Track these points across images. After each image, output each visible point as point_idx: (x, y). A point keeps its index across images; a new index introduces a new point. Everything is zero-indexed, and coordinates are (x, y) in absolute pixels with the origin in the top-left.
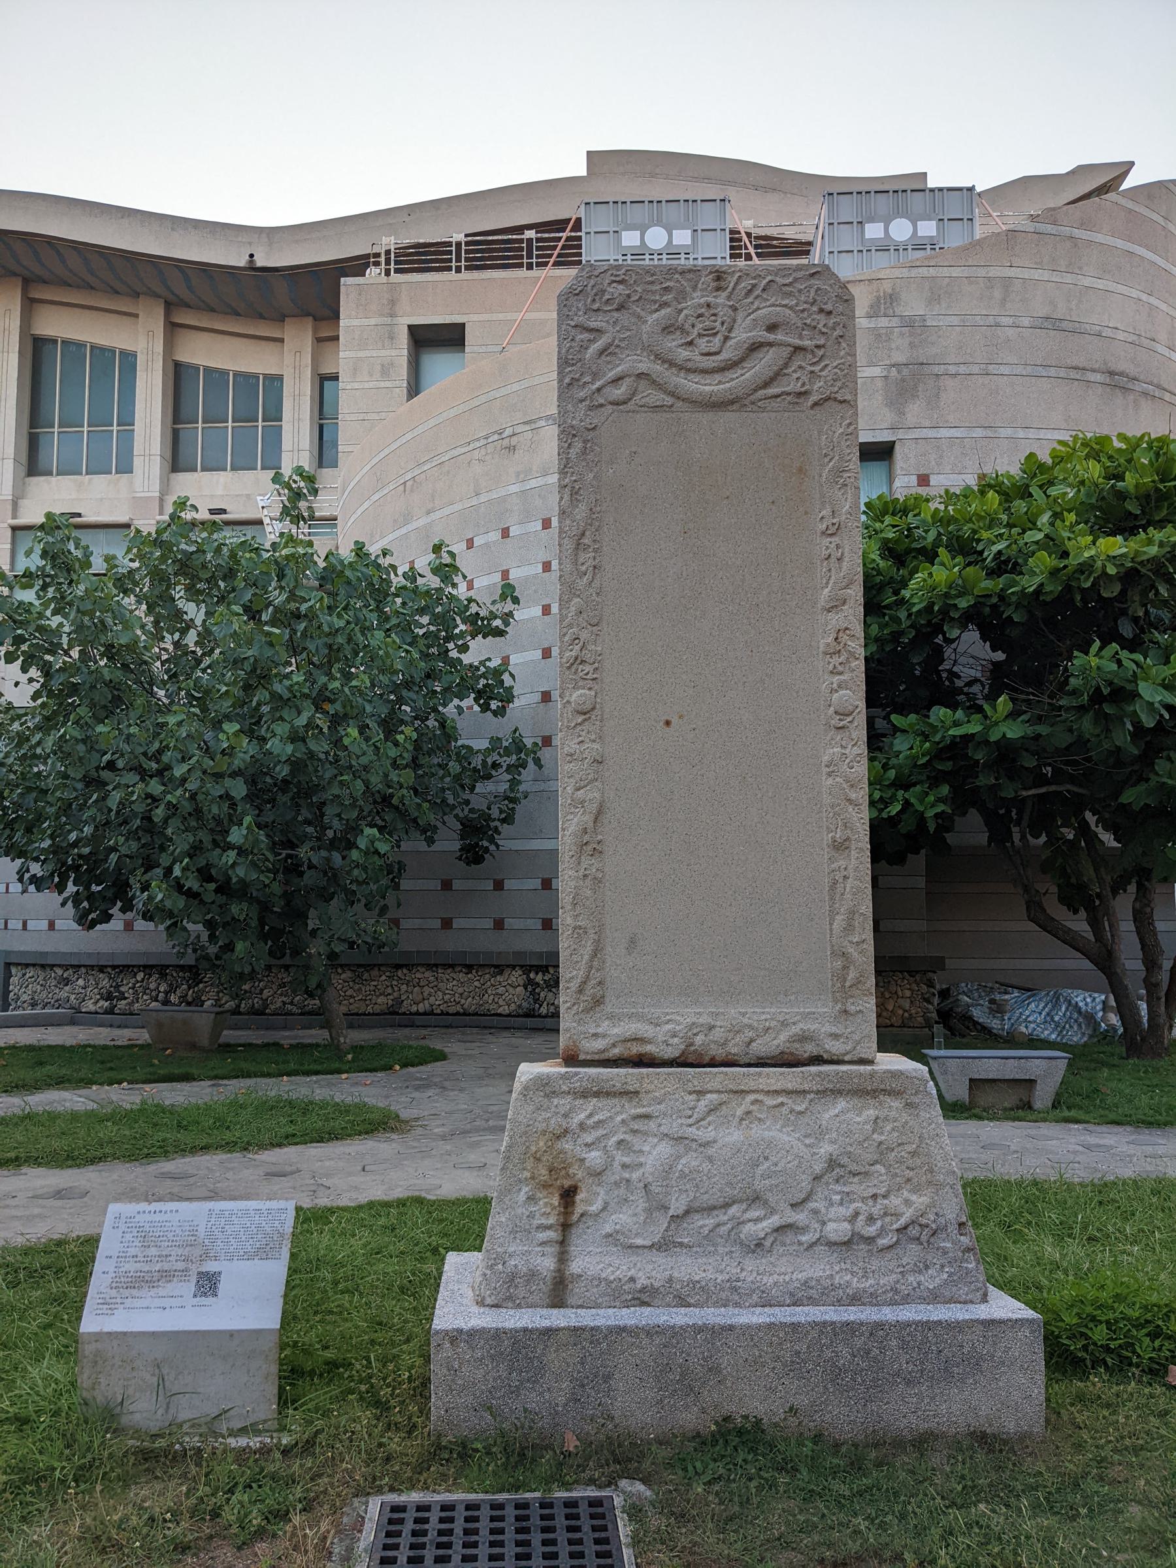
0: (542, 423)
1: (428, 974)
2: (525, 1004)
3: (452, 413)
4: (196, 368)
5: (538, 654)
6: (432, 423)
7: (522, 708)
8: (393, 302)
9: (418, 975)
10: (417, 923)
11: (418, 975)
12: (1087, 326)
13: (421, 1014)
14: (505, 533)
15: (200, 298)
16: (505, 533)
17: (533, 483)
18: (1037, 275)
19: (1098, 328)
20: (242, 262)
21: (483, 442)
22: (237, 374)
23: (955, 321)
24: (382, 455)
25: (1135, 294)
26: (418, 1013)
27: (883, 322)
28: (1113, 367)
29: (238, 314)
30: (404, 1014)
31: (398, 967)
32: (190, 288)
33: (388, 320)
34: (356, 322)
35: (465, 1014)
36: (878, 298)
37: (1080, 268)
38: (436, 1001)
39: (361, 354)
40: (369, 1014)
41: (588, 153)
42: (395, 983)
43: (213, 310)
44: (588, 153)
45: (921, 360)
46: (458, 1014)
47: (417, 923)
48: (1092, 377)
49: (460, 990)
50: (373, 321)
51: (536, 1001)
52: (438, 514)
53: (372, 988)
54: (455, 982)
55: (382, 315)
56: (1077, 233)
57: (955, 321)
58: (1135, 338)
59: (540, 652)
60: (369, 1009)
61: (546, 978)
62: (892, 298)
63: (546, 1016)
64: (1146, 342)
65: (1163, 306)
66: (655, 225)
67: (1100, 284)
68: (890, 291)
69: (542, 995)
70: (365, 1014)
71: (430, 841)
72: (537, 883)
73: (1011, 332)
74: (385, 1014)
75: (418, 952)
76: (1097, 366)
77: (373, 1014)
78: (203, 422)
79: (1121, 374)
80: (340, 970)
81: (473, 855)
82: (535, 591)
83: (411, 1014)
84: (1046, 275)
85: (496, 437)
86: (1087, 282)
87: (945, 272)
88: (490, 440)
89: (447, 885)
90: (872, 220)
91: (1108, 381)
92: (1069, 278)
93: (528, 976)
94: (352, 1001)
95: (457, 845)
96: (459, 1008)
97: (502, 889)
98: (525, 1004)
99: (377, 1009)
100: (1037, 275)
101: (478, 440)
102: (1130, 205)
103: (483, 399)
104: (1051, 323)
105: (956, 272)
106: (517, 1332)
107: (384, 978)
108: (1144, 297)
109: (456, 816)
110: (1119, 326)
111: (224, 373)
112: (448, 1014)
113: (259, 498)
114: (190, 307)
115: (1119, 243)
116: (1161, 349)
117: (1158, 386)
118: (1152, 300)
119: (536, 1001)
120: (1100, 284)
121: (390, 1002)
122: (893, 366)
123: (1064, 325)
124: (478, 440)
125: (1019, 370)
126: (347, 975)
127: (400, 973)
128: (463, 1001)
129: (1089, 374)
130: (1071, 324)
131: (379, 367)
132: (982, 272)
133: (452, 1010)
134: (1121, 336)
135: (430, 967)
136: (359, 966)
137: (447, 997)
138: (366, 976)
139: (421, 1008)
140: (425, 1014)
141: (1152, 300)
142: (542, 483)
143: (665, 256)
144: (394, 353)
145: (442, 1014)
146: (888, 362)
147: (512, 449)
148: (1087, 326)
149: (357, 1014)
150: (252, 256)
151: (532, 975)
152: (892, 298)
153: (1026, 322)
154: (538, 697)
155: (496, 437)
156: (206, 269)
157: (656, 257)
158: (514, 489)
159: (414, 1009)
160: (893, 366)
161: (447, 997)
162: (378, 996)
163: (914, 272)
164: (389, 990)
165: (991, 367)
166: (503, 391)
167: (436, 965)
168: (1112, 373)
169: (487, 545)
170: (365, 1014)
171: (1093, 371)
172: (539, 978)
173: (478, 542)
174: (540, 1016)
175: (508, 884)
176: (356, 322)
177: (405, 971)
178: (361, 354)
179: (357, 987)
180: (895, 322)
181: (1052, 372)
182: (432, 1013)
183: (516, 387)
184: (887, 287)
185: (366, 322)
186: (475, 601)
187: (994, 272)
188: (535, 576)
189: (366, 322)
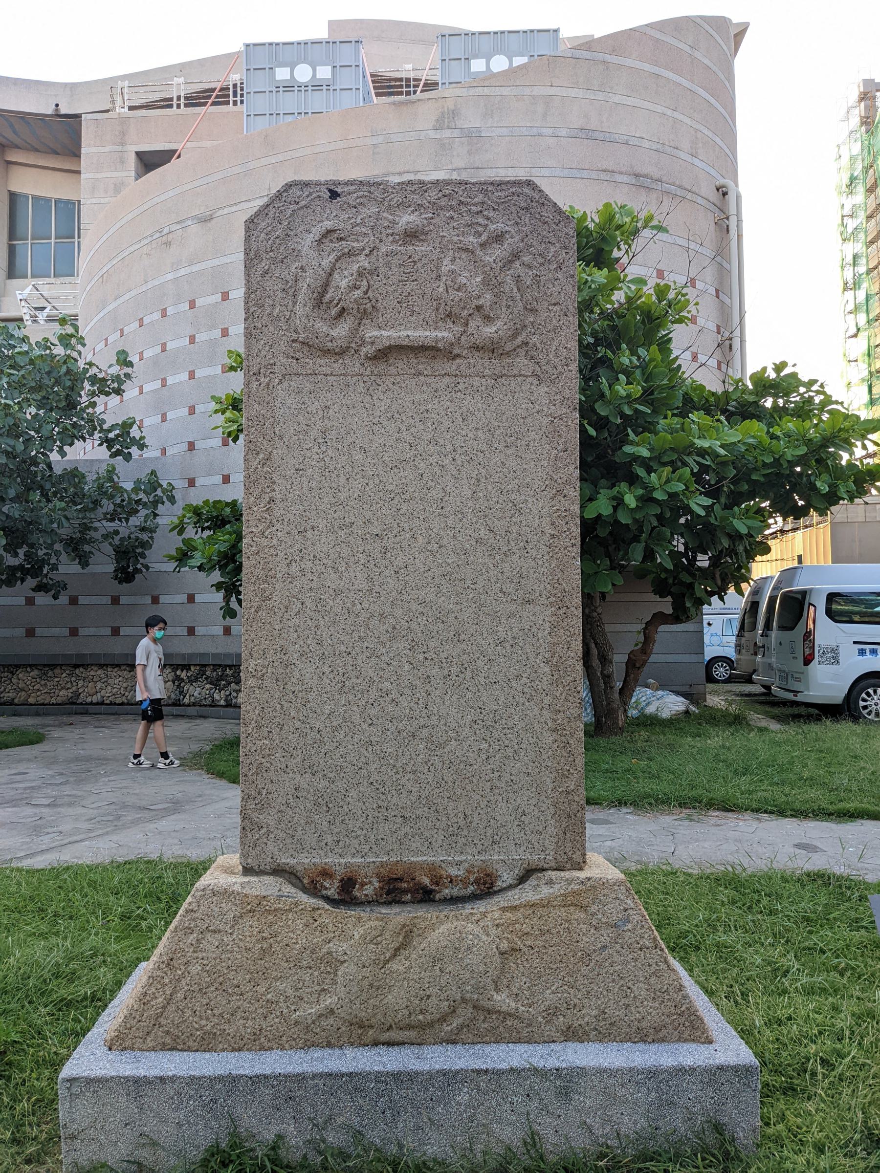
0: (189, 222)
1: (100, 672)
2: (173, 696)
3: (130, 216)
4: (26, 197)
5: (186, 411)
6: (118, 225)
7: (173, 455)
8: (123, 134)
9: (92, 673)
10: (92, 631)
11: (92, 673)
12: (616, 136)
13: (95, 704)
14: (164, 314)
15: (26, 142)
16: (164, 314)
17: (182, 272)
18: (573, 93)
19: (626, 138)
20: (50, 111)
21: (150, 239)
22: (57, 201)
23: (505, 131)
24: (91, 254)
25: (659, 109)
26: (91, 703)
27: (447, 134)
28: (639, 170)
29: (58, 154)
30: (81, 704)
31: (76, 666)
32: (15, 132)
33: (119, 148)
34: (94, 150)
35: (128, 704)
36: (443, 113)
37: (611, 88)
38: (106, 694)
39: (98, 176)
40: (53, 704)
41: (329, 22)
42: (73, 679)
43: (37, 150)
44: (329, 22)
45: (476, 166)
46: (122, 704)
47: (92, 631)
48: (619, 178)
49: (125, 685)
50: (107, 149)
51: (181, 692)
52: (122, 299)
53: (55, 683)
54: (121, 679)
55: (114, 144)
56: (608, 58)
57: (505, 131)
58: (659, 146)
59: (187, 409)
60: (53, 701)
61: (189, 675)
62: (454, 113)
63: (189, 705)
64: (669, 150)
65: (688, 121)
66: (303, 63)
67: (629, 101)
68: (452, 108)
69: (185, 688)
70: (50, 705)
71: (84, 564)
72: (184, 598)
73: (552, 140)
74: (66, 704)
75: (104, 655)
76: (624, 170)
77: (56, 704)
78: (32, 239)
79: (645, 176)
80: (29, 669)
81: (125, 575)
82: (184, 360)
83: (87, 704)
84: (581, 93)
85: (158, 235)
86: (617, 99)
87: (498, 91)
88: (154, 237)
89: (115, 600)
90: (476, 57)
91: (633, 182)
92: (600, 96)
93: (175, 674)
94: (39, 693)
95: (111, 568)
96: (124, 700)
97: (158, 603)
98: (173, 696)
99: (59, 700)
100: (573, 93)
101: (146, 238)
102: (658, 35)
103: (149, 204)
104: (586, 134)
105: (506, 91)
106: (784, 880)
107: (64, 675)
108: (669, 112)
109: (110, 544)
110: (644, 136)
111: (48, 200)
112: (115, 704)
113: (17, 292)
114: (19, 148)
115: (647, 67)
116: (682, 155)
117: (680, 187)
118: (676, 115)
119: (181, 692)
120: (629, 101)
121: (70, 695)
122: (455, 170)
123: (596, 135)
124: (146, 238)
125: (557, 172)
126: (35, 673)
127: (77, 671)
128: (127, 694)
129: (617, 175)
130: (602, 134)
131: (113, 186)
132: (527, 91)
133: (119, 701)
134: (647, 144)
135: (101, 666)
136: (45, 666)
137: (115, 690)
138: (50, 673)
139: (95, 699)
140: (98, 704)
141: (676, 115)
142: (189, 271)
143: (310, 88)
144: (125, 174)
145: (111, 704)
146: (450, 167)
147: (168, 244)
148: (616, 136)
149: (43, 704)
150: (57, 105)
151: (178, 673)
152: (454, 113)
153: (564, 132)
154: (185, 447)
155: (158, 235)
156: (23, 116)
157: (303, 88)
158: (170, 276)
159: (89, 700)
160: (455, 170)
161: (115, 690)
162: (60, 690)
163: (472, 92)
164: (69, 685)
165: (533, 170)
166: (163, 197)
167: (107, 665)
168: (637, 175)
169: (211, 328)
170: (50, 705)
171: (621, 173)
172: (184, 675)
173: (146, 321)
174: (184, 705)
175: (162, 599)
176: (94, 150)
177: (82, 670)
178: (98, 176)
179: (43, 682)
180: (456, 133)
181: (585, 174)
182: (102, 703)
183: (171, 194)
184: (450, 104)
185: (102, 149)
186: (94, 364)
187: (537, 91)
188: (184, 347)
189: (102, 149)
